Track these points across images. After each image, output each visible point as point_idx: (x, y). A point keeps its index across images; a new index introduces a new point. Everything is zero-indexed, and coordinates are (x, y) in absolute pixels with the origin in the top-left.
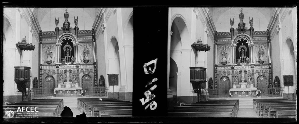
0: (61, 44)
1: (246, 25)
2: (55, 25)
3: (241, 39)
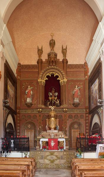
0: (45, 82)
1: (58, 55)
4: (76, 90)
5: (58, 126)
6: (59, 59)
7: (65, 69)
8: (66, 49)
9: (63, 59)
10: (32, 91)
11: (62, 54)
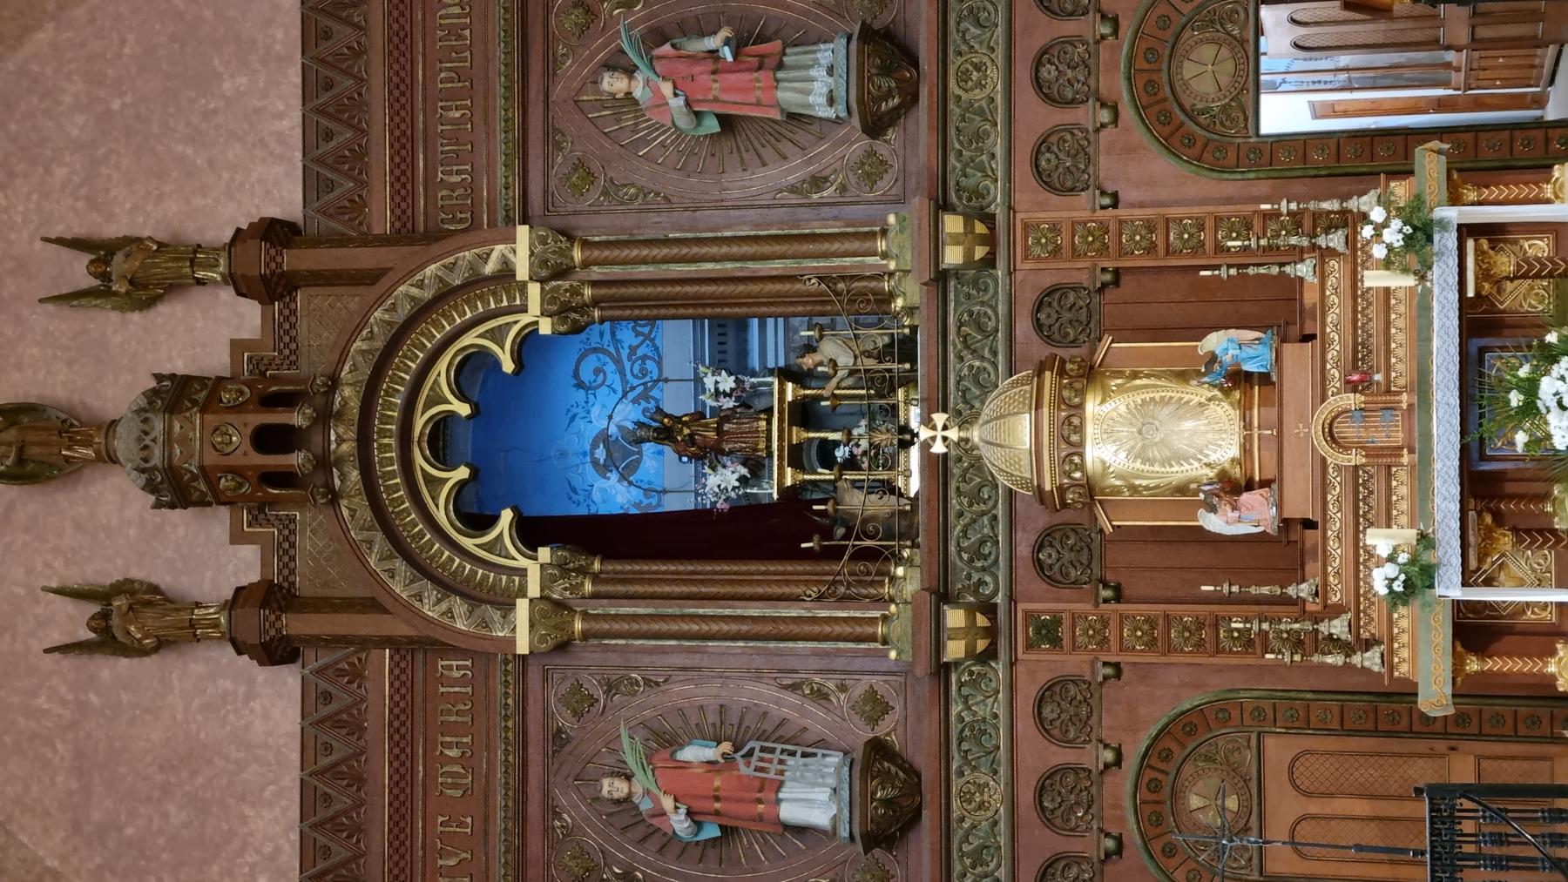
0: (544, 553)
1: (180, 367)
4: (668, 803)
5: (1215, 342)
6: (237, 346)
7: (365, 258)
8: (101, 251)
9: (227, 294)
10: (682, 747)
11: (163, 309)
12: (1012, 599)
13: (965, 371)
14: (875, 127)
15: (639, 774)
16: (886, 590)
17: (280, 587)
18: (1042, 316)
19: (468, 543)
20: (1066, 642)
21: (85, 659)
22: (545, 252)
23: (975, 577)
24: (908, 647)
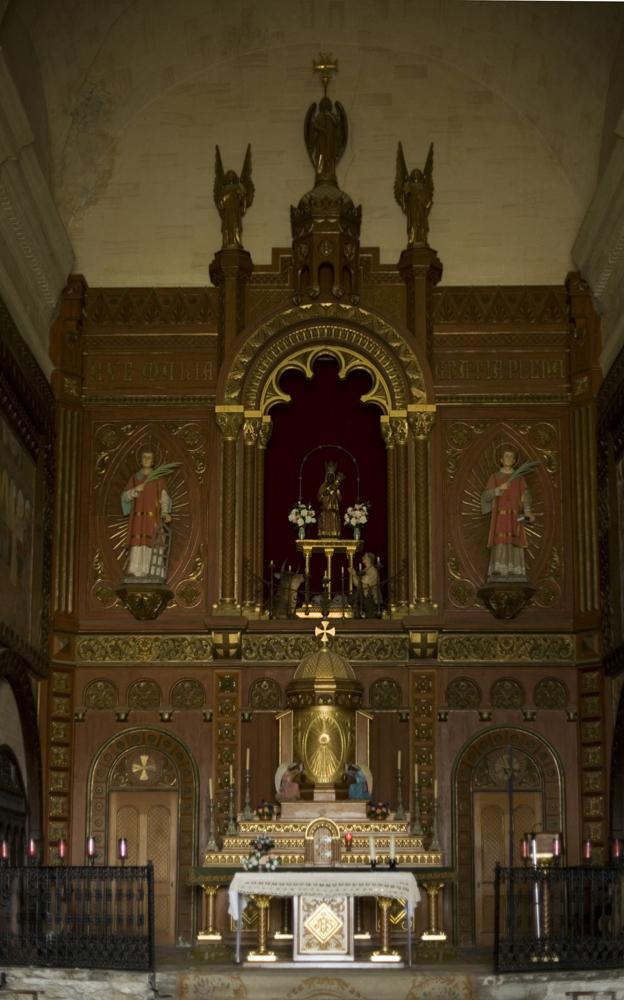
0: (267, 419)
2: (216, 223)
3: (317, 365)
4: (140, 488)
6: (376, 251)
8: (425, 177)
10: (169, 494)
12: (247, 667)
13: (358, 643)
14: (485, 595)
15: (156, 472)
16: (248, 603)
17: (250, 275)
18: (385, 683)
19: (273, 377)
20: (222, 694)
21: (213, 165)
22: (423, 420)
23: (254, 648)
24: (220, 613)
